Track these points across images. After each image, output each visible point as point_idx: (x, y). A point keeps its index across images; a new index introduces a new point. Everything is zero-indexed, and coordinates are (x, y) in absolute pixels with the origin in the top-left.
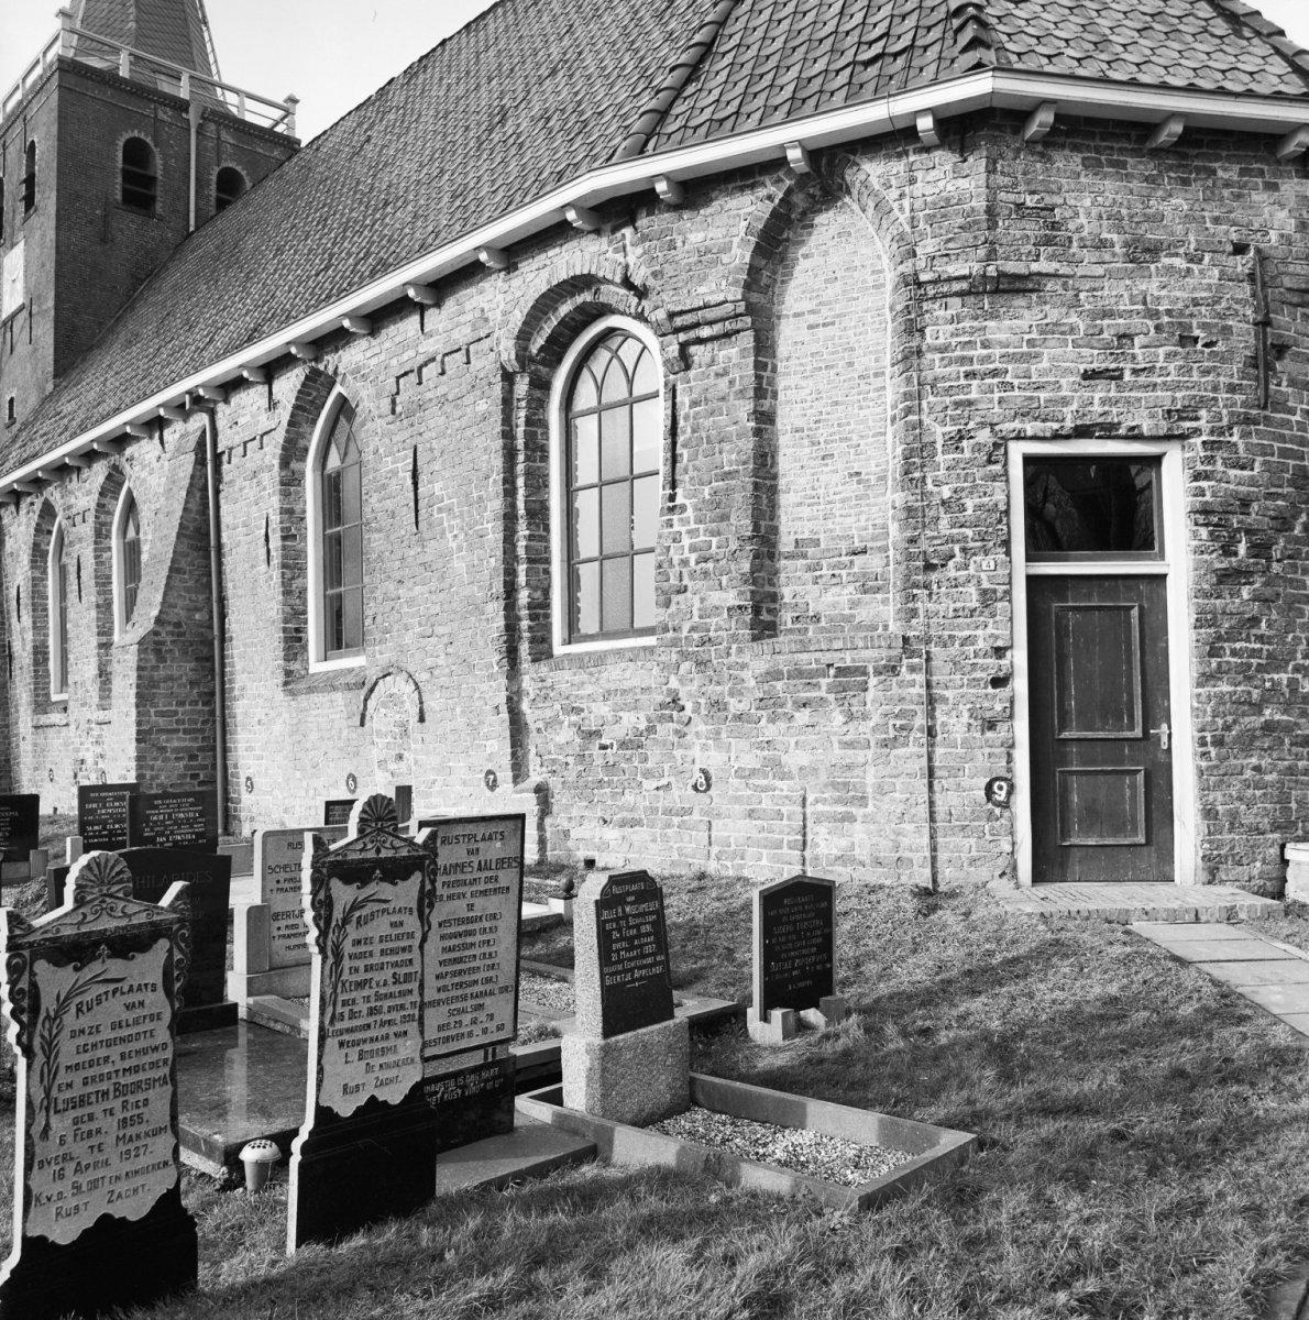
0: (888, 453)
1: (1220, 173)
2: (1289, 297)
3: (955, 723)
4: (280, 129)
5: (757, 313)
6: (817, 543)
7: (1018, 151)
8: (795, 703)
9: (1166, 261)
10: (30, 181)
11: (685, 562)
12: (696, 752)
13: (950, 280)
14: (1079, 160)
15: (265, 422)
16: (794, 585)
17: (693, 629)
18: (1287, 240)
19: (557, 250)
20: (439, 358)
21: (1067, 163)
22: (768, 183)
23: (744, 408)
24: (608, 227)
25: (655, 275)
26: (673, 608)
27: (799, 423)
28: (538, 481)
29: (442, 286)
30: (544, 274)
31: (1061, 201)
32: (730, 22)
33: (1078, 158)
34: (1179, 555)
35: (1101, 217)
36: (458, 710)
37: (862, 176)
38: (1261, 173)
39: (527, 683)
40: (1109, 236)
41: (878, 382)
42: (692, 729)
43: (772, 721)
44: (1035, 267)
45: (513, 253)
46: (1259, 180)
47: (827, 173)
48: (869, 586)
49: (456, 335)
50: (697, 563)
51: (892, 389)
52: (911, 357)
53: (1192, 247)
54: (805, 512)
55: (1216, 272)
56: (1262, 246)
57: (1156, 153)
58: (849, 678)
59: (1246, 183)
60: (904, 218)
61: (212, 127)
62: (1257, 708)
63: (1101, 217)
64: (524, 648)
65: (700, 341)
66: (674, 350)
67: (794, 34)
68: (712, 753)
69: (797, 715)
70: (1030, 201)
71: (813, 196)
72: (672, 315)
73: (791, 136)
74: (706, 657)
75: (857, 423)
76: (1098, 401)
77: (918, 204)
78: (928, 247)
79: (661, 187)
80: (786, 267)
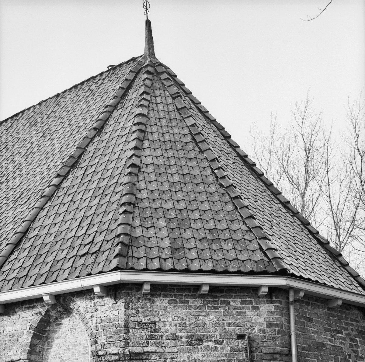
1: (232, 303)
2: (266, 357)
7: (139, 299)
9: (206, 344)
13: (110, 355)
14: (167, 301)
18: (262, 331)
21: (161, 302)
22: (39, 307)
31: (158, 320)
32: (37, 220)
33: (166, 300)
35: (176, 326)
37: (76, 307)
38: (251, 302)
40: (180, 334)
44: (146, 349)
46: (250, 306)
47: (63, 303)
53: (218, 337)
55: (229, 348)
56: (251, 335)
57: (202, 296)
59: (244, 307)
60: (93, 326)
63: (176, 326)
67: (59, 233)
70: (144, 320)
71: (60, 312)
77: (99, 320)
78: (102, 340)
80: (49, 342)
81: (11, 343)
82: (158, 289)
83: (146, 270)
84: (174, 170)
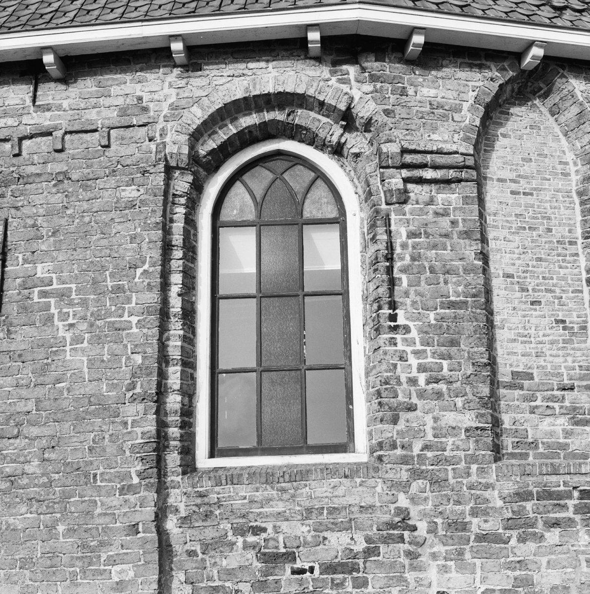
5: (471, 171)
6: (530, 377)
8: (545, 523)
11: (413, 381)
17: (426, 447)
19: (263, 64)
20: (59, 134)
24: (329, 58)
25: (387, 113)
26: (401, 425)
27: (510, 270)
29: (77, 65)
36: (61, 528)
39: (175, 498)
41: (572, 249)
42: (426, 551)
43: (522, 540)
45: (202, 54)
50: (428, 382)
54: (519, 348)
64: (173, 459)
65: (420, 181)
68: (454, 574)
69: (547, 535)
72: (404, 151)
74: (442, 475)
75: (558, 279)
79: (48, 59)
81: (436, 118)
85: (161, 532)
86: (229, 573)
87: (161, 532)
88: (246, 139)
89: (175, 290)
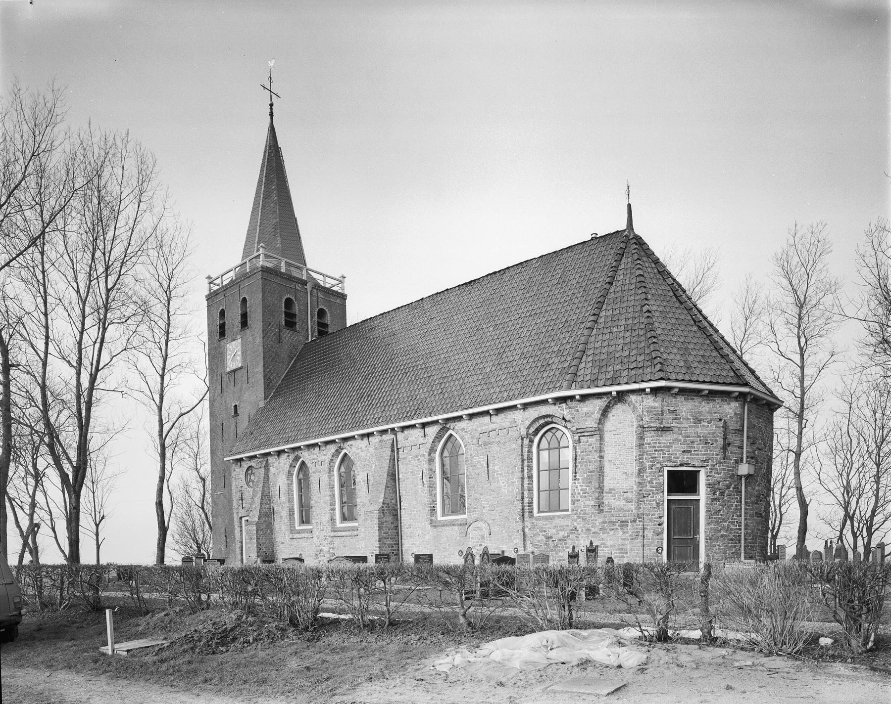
0: (634, 468)
3: (649, 534)
4: (335, 289)
5: (599, 431)
10: (244, 316)
12: (582, 542)
15: (421, 440)
16: (608, 500)
21: (681, 399)
23: (596, 455)
28: (530, 469)
29: (498, 411)
30: (537, 412)
34: (703, 494)
45: (526, 406)
47: (621, 396)
48: (628, 501)
49: (504, 424)
51: (635, 453)
52: (640, 445)
57: (701, 396)
58: (624, 523)
61: (315, 291)
62: (720, 531)
64: (526, 515)
66: (577, 438)
73: (614, 389)
76: (685, 458)
78: (646, 419)
82: (682, 391)
83: (676, 380)
84: (670, 315)
85: (524, 532)
86: (539, 541)
87: (524, 532)
88: (542, 426)
89: (526, 472)
